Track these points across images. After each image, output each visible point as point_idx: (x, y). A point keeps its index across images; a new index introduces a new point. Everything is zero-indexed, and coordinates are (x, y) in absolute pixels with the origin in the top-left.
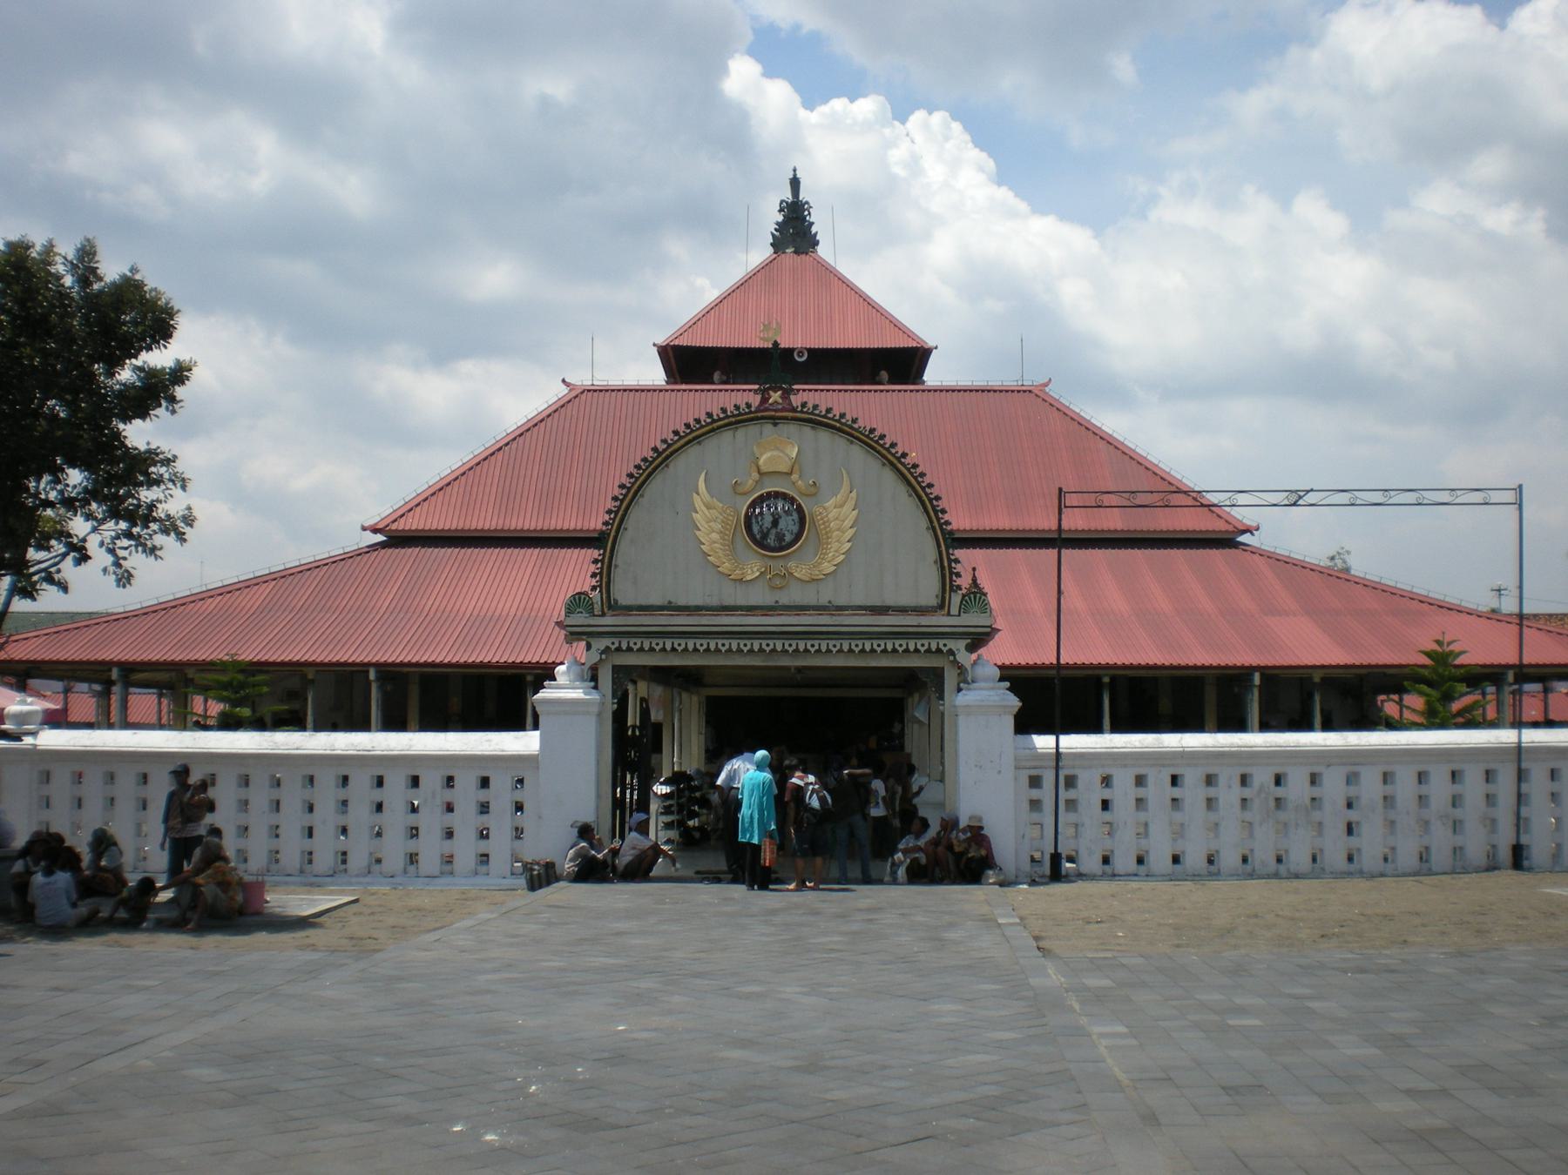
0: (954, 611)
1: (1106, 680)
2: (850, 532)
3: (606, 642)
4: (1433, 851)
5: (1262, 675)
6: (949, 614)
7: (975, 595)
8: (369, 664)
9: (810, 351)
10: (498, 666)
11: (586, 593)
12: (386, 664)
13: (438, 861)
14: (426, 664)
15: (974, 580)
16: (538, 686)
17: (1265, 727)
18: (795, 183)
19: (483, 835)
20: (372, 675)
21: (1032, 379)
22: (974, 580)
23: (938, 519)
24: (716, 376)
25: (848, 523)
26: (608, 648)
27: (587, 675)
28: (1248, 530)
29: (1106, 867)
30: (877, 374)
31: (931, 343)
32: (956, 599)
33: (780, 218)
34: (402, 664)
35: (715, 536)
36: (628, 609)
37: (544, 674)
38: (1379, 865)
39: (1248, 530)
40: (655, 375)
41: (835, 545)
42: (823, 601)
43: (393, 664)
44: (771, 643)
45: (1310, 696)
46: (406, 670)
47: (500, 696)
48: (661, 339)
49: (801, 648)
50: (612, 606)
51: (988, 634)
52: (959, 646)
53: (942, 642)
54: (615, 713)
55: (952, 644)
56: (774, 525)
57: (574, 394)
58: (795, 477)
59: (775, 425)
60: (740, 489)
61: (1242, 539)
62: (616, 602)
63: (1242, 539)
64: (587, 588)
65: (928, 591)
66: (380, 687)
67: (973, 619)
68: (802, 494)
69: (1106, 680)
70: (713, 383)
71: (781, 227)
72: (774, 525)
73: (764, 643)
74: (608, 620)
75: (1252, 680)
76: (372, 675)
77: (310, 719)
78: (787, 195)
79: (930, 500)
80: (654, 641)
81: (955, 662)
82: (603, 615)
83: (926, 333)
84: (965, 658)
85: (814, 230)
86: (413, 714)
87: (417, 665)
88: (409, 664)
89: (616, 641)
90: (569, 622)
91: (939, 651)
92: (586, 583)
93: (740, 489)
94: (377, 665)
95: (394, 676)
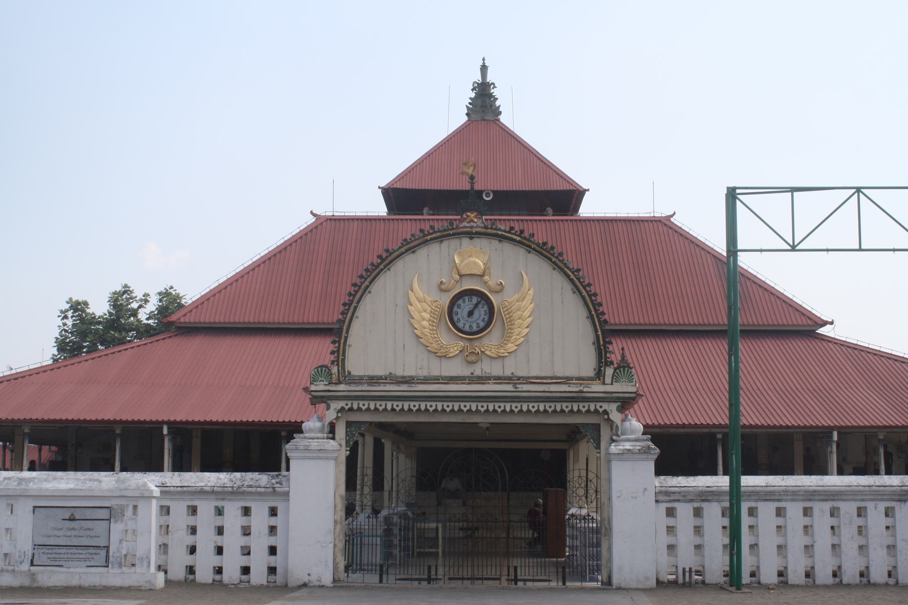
0: (608, 380)
1: (719, 436)
2: (526, 331)
3: (342, 404)
4: (872, 569)
5: (839, 433)
6: (604, 383)
7: (623, 368)
8: (163, 422)
9: (494, 192)
10: (260, 424)
11: (326, 367)
12: (175, 422)
13: (239, 571)
14: (206, 423)
15: (623, 356)
16: (289, 438)
17: (841, 472)
18: (484, 69)
19: (246, 551)
20: (165, 431)
21: (661, 212)
22: (623, 356)
23: (596, 310)
24: (425, 210)
25: (527, 313)
26: (343, 408)
27: (327, 429)
28: (825, 323)
29: (244, 577)
30: (545, 210)
31: (585, 187)
32: (609, 371)
33: (473, 95)
34: (187, 422)
35: (425, 323)
36: (359, 380)
37: (295, 428)
38: (830, 581)
39: (825, 323)
40: (379, 208)
41: (517, 331)
42: (508, 373)
43: (181, 422)
44: (468, 404)
45: (876, 451)
46: (190, 427)
47: (257, 447)
48: (386, 179)
49: (491, 409)
50: (346, 377)
51: (634, 399)
52: (612, 408)
53: (598, 405)
54: (348, 458)
55: (605, 406)
56: (471, 312)
57: (320, 221)
58: (486, 278)
59: (471, 238)
60: (443, 287)
61: (822, 331)
62: (349, 373)
63: (822, 331)
64: (327, 362)
65: (588, 366)
66: (173, 441)
67: (623, 387)
68: (491, 291)
69: (719, 436)
70: (422, 214)
71: (473, 101)
72: (471, 312)
73: (462, 404)
74: (342, 387)
75: (832, 437)
76: (165, 431)
77: (117, 464)
78: (478, 78)
79: (590, 296)
80: (378, 403)
81: (609, 420)
82: (339, 382)
83: (580, 178)
84: (616, 416)
85: (497, 104)
86: (196, 459)
87: (199, 423)
88: (193, 423)
89: (349, 403)
90: (313, 388)
91: (596, 411)
92: (327, 359)
93: (443, 287)
94: (169, 423)
95: (183, 432)
